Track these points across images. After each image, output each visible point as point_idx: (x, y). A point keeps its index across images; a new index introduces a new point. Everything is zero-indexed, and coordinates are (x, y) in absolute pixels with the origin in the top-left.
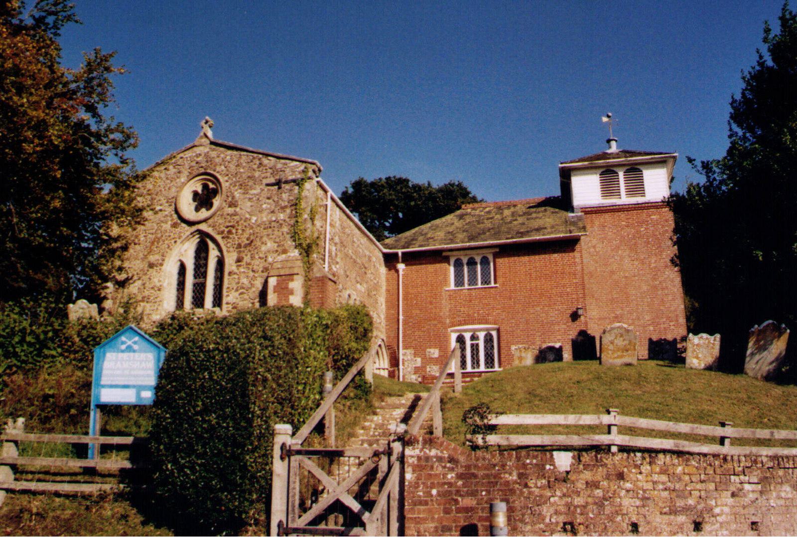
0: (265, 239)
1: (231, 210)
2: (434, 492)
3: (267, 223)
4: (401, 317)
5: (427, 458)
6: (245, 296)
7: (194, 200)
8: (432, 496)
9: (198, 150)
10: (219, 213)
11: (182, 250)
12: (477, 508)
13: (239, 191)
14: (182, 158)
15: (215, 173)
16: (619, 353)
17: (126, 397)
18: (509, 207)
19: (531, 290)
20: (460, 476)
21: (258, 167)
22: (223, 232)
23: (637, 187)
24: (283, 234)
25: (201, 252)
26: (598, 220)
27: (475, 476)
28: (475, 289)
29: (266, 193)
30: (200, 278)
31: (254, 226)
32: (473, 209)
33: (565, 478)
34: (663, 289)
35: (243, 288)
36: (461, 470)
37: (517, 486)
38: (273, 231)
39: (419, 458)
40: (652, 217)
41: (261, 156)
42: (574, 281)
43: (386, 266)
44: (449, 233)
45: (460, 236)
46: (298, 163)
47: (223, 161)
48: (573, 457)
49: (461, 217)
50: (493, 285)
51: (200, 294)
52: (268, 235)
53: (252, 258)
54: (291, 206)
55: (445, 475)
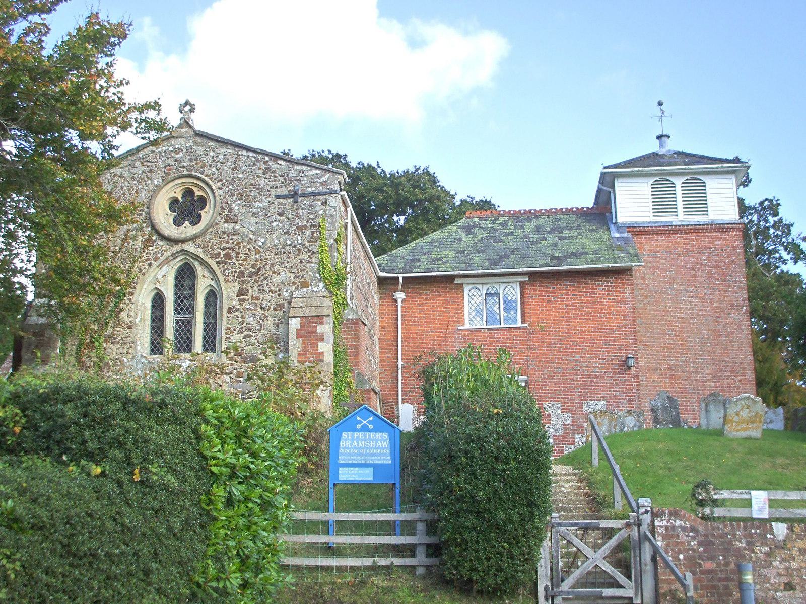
0: (277, 267)
1: (228, 227)
2: (681, 557)
3: (280, 247)
4: (400, 363)
5: (674, 528)
6: (252, 340)
7: (172, 209)
8: (679, 560)
9: (177, 143)
10: (211, 229)
11: (160, 276)
12: (717, 571)
13: (239, 202)
14: (153, 152)
15: (203, 176)
16: (744, 426)
17: (366, 475)
18: (529, 220)
19: (569, 333)
20: (700, 544)
21: (264, 173)
22: (218, 255)
23: (699, 203)
24: (301, 262)
25: (185, 276)
26: (648, 244)
27: (713, 543)
28: (497, 329)
29: (274, 209)
30: (184, 313)
31: (262, 250)
32: (481, 219)
33: (783, 546)
34: (727, 335)
35: (250, 330)
36: (701, 539)
37: (746, 552)
38: (289, 257)
39: (667, 528)
40: (716, 243)
41: (267, 158)
42: (623, 322)
43: (381, 294)
44: (459, 252)
45: (478, 258)
46: (318, 171)
47: (214, 160)
48: (788, 528)
49: (468, 229)
50: (519, 324)
51: (185, 334)
52: (282, 263)
53: (261, 291)
54: (312, 226)
55: (689, 543)
